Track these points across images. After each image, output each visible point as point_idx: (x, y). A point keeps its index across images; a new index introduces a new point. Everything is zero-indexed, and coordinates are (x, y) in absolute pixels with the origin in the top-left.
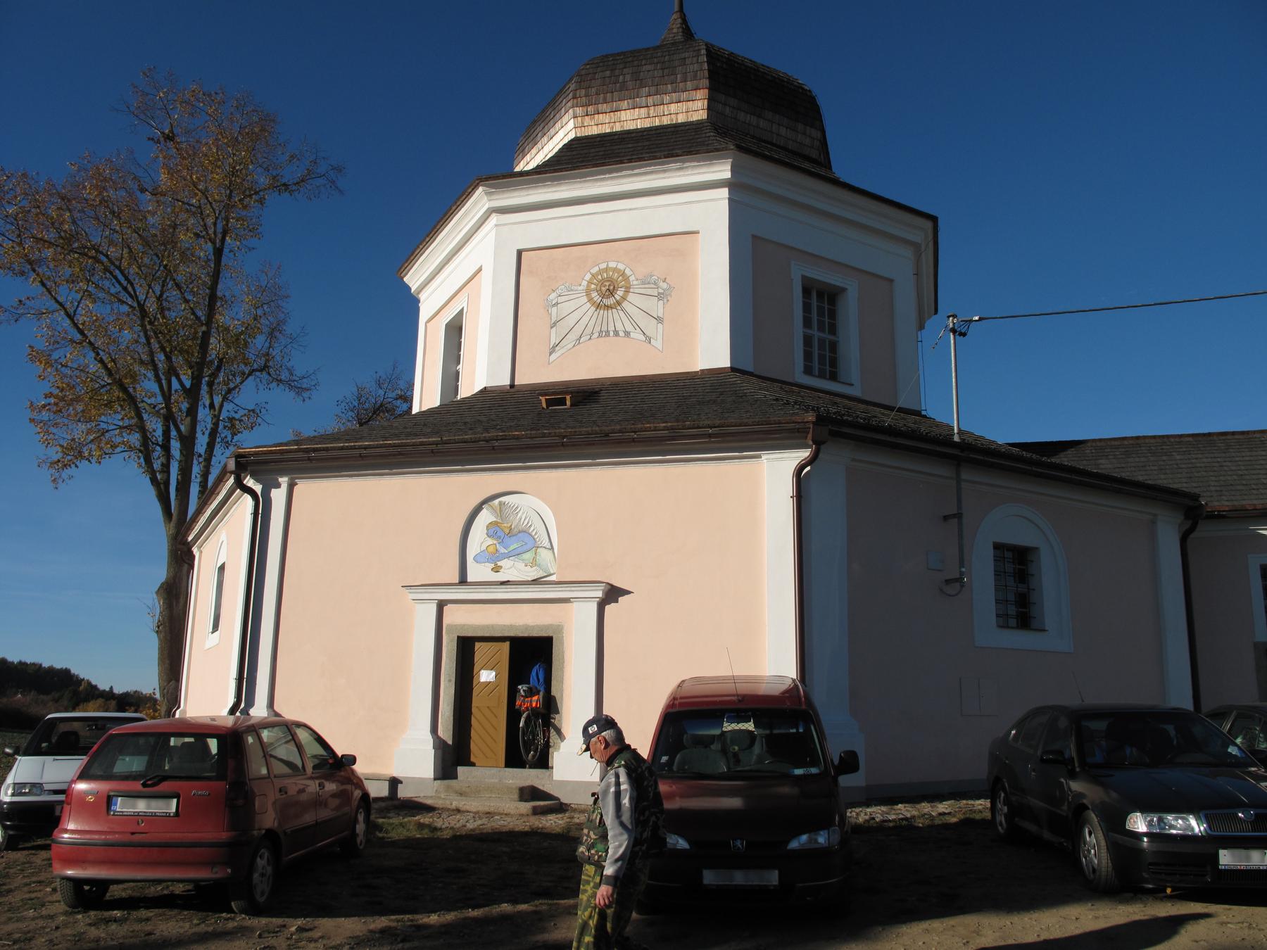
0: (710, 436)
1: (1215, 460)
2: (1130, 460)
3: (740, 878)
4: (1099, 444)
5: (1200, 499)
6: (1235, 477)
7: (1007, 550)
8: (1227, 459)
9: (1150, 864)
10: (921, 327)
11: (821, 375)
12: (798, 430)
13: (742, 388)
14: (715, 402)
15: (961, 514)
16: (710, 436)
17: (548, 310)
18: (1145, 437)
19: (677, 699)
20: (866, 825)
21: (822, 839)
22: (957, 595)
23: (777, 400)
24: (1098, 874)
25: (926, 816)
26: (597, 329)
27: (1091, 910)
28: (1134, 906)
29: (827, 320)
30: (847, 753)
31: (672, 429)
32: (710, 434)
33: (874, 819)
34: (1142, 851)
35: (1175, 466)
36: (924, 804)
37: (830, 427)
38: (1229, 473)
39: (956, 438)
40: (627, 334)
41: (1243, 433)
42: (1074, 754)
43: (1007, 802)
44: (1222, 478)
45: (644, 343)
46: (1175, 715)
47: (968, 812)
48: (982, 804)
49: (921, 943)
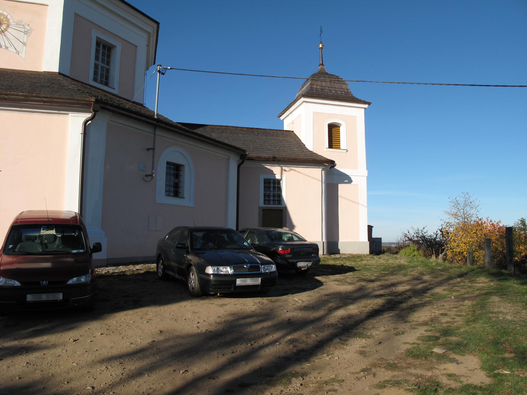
0: (44, 102)
1: (253, 138)
2: (223, 134)
3: (44, 297)
4: (212, 127)
5: (246, 152)
6: (259, 145)
7: (172, 165)
8: (257, 138)
9: (213, 285)
10: (147, 69)
11: (101, 83)
12: (87, 104)
13: (63, 83)
14: (49, 87)
15: (155, 148)
16: (44, 102)
18: (229, 126)
19: (19, 220)
20: (106, 274)
21: (83, 279)
22: (150, 181)
23: (79, 90)
24: (194, 290)
25: (131, 271)
27: (191, 303)
28: (206, 301)
29: (106, 58)
30: (97, 243)
31: (26, 96)
32: (45, 101)
33: (109, 272)
34: (209, 280)
35: (239, 139)
36: (130, 266)
37: (101, 105)
38: (257, 143)
39: (156, 117)
40: (7, 48)
41: (264, 129)
42: (189, 245)
43: (163, 264)
44: (255, 145)
45: (5, 50)
46: (229, 232)
47: (148, 269)
48: (154, 265)
49: (123, 320)
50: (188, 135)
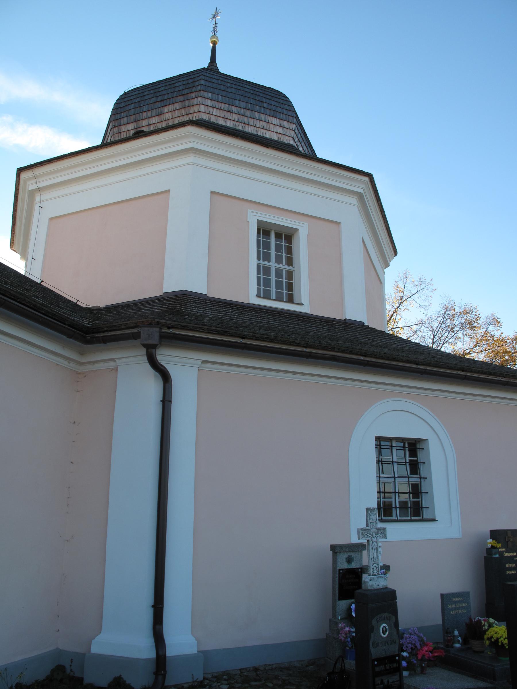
11: (279, 299)
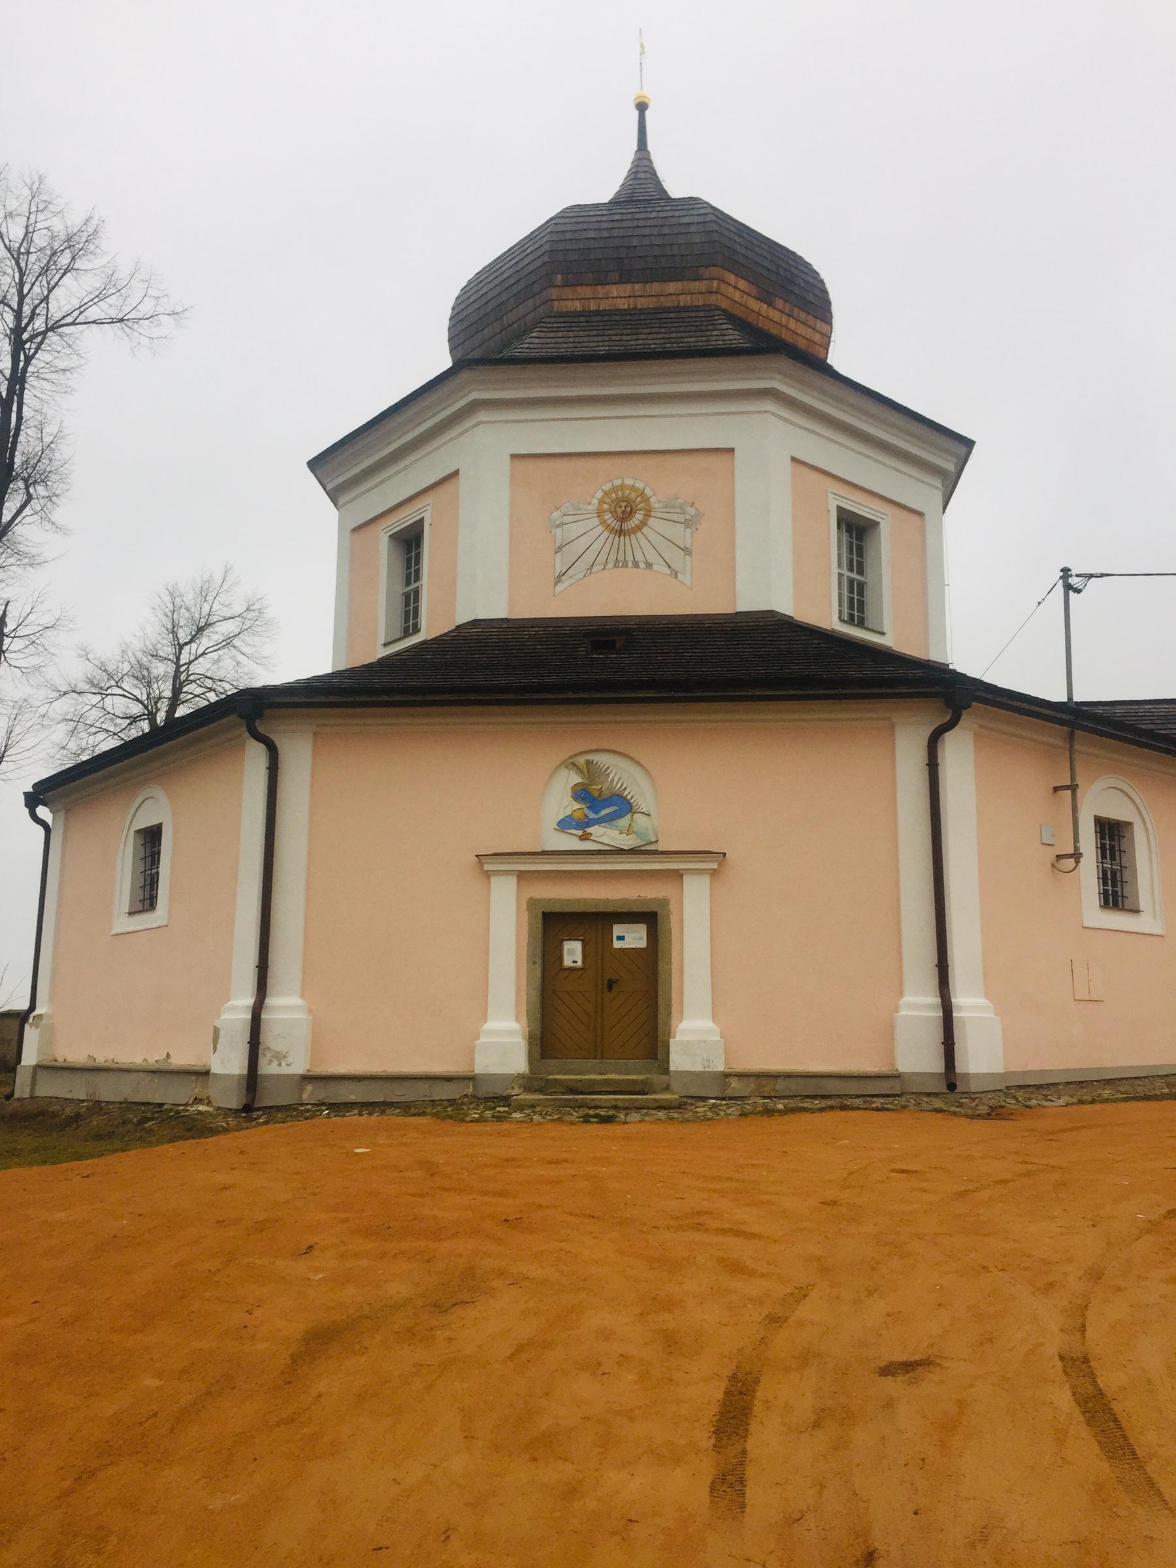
17: (551, 532)
26: (613, 557)
40: (649, 565)
50: (828, 689)
